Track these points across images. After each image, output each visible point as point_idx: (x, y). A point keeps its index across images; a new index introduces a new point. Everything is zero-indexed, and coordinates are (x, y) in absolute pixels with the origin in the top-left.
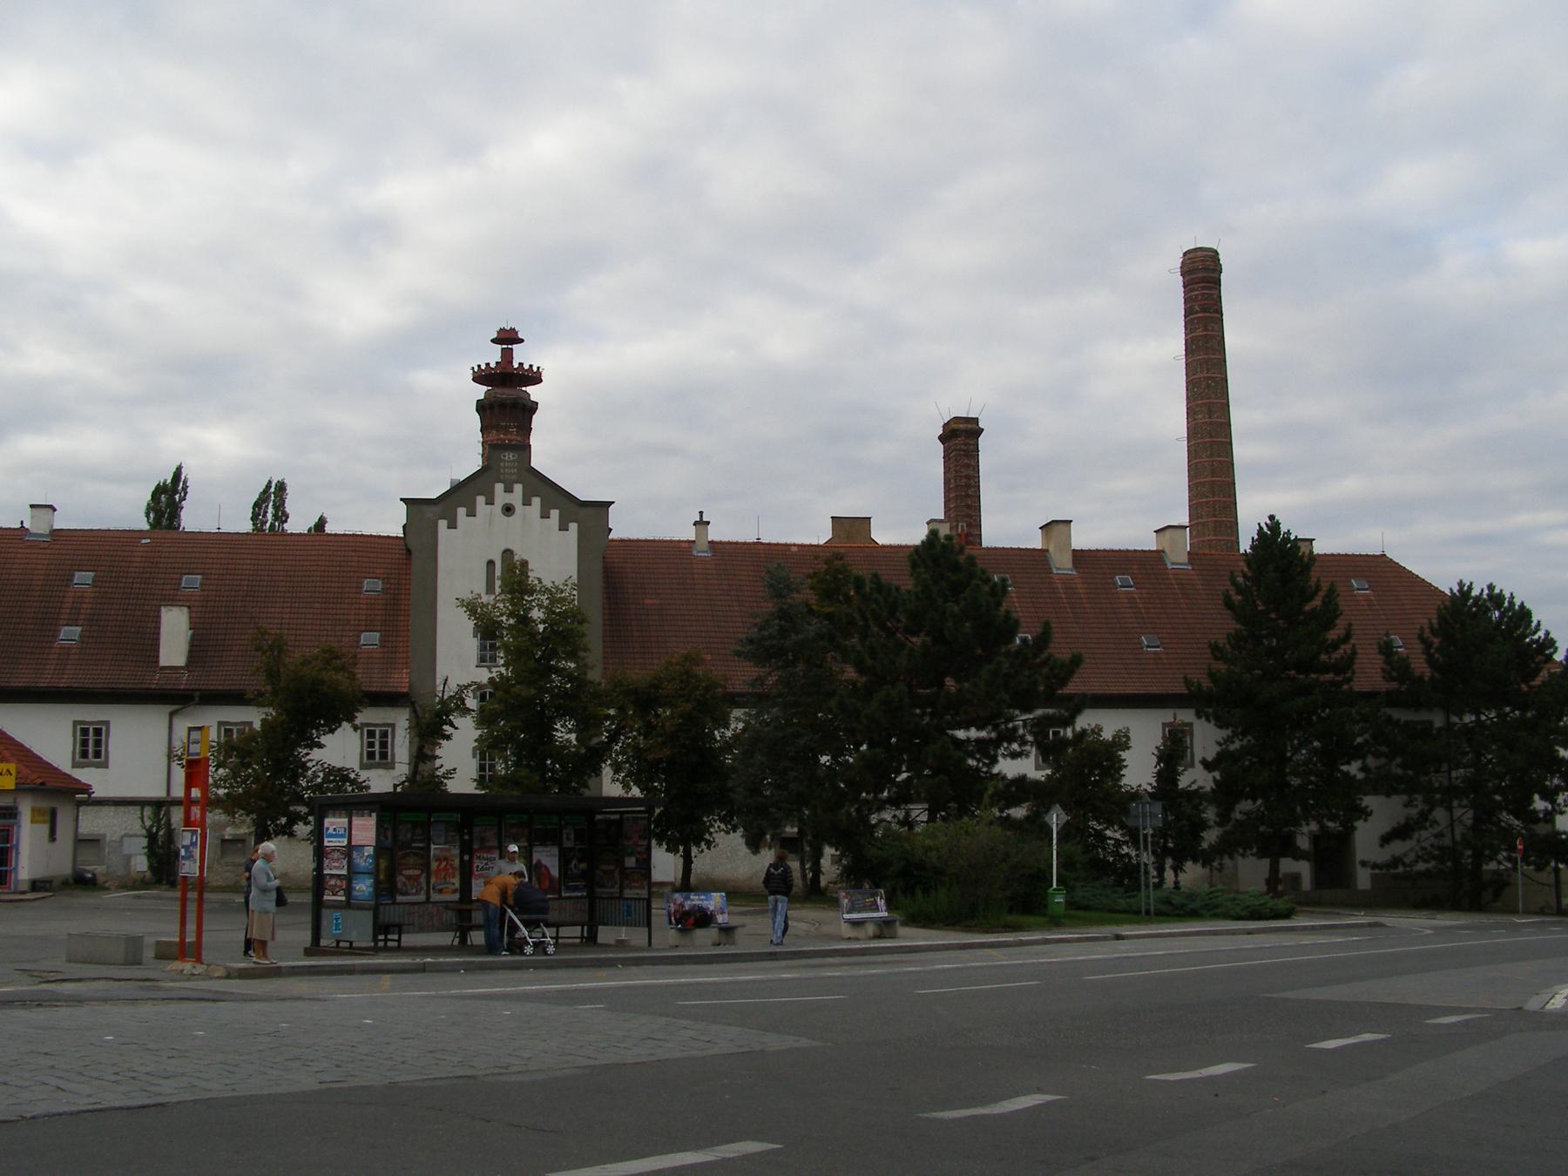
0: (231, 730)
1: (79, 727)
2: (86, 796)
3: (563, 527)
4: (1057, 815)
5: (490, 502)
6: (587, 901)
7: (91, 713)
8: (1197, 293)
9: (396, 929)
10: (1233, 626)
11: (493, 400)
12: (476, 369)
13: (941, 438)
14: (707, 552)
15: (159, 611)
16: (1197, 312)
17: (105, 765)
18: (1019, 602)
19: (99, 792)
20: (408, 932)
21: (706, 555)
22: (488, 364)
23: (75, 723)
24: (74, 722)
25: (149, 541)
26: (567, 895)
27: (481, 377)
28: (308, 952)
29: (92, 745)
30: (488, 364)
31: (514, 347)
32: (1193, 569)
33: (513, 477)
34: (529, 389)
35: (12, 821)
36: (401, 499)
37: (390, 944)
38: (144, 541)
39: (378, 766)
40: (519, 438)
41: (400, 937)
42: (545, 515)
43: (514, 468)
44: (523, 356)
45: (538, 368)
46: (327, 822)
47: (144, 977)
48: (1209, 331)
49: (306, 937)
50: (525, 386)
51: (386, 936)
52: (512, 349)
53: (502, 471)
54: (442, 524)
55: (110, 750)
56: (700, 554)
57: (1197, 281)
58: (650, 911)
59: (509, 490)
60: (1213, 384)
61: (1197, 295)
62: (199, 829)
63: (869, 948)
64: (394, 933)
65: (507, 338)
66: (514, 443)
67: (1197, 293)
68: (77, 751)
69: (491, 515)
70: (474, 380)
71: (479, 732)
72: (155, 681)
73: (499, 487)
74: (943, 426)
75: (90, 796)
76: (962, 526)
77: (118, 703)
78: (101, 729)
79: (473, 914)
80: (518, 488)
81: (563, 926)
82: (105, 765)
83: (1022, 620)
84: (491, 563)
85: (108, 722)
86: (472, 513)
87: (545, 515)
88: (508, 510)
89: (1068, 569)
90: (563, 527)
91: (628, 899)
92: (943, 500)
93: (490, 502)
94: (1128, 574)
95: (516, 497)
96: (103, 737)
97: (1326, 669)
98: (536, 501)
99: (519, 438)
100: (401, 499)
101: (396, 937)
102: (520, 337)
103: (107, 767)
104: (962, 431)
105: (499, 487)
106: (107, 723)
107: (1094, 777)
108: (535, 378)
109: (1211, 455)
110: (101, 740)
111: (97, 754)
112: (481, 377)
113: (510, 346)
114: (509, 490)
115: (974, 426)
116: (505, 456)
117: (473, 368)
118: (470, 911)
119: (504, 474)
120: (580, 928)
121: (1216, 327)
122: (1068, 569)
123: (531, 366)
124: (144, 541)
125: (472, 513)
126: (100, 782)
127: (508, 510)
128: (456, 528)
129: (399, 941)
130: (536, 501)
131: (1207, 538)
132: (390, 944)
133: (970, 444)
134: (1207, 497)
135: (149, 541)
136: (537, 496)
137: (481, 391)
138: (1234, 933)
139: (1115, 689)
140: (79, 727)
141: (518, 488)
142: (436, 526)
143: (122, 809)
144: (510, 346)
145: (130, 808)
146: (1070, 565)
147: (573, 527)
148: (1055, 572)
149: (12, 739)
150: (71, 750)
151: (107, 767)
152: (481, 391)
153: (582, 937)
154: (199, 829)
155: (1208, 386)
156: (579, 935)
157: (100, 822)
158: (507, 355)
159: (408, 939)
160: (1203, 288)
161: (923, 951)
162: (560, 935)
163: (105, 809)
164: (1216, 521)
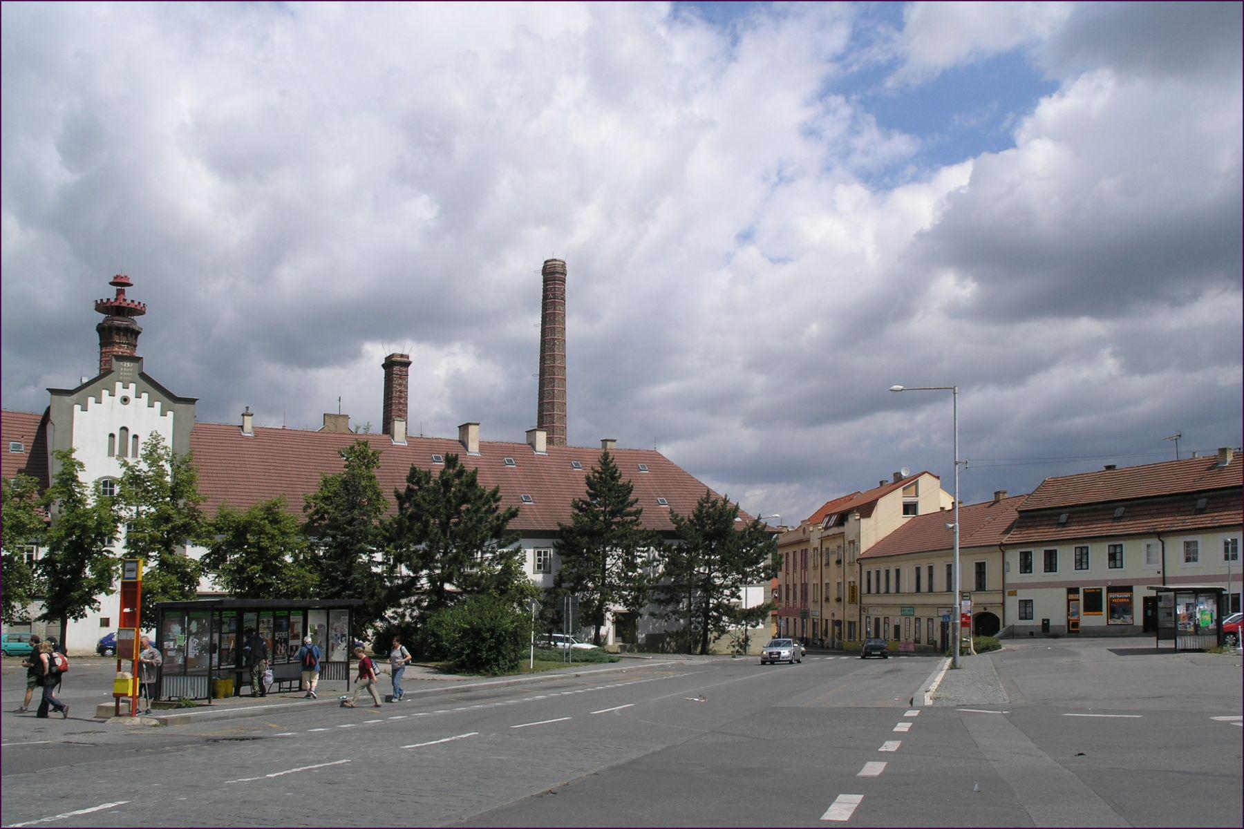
3: (163, 414)
5: (112, 394)
10: (488, 490)
12: (99, 302)
13: (383, 366)
14: (250, 433)
16: (551, 299)
21: (250, 435)
22: (102, 300)
27: (101, 307)
30: (108, 299)
31: (126, 288)
34: (136, 318)
36: (47, 389)
40: (129, 351)
42: (151, 405)
43: (130, 372)
46: (245, 617)
47: (231, 736)
52: (124, 290)
53: (121, 374)
54: (77, 408)
55: (533, 557)
58: (349, 671)
63: (479, 687)
65: (120, 284)
66: (124, 354)
69: (113, 403)
70: (96, 309)
71: (126, 551)
73: (119, 385)
74: (386, 358)
79: (243, 674)
80: (132, 386)
81: (294, 680)
83: (405, 481)
84: (112, 435)
86: (99, 401)
87: (151, 405)
88: (125, 400)
89: (476, 453)
90: (163, 414)
91: (334, 663)
92: (383, 404)
93: (112, 394)
97: (630, 514)
99: (129, 351)
100: (47, 389)
105: (119, 385)
107: (188, 578)
112: (101, 307)
115: (406, 359)
118: (241, 673)
119: (123, 376)
121: (561, 308)
122: (476, 453)
125: (99, 401)
127: (125, 400)
130: (145, 396)
136: (106, 389)
137: (101, 317)
141: (132, 386)
142: (72, 409)
146: (477, 451)
147: (170, 414)
152: (101, 317)
158: (120, 292)
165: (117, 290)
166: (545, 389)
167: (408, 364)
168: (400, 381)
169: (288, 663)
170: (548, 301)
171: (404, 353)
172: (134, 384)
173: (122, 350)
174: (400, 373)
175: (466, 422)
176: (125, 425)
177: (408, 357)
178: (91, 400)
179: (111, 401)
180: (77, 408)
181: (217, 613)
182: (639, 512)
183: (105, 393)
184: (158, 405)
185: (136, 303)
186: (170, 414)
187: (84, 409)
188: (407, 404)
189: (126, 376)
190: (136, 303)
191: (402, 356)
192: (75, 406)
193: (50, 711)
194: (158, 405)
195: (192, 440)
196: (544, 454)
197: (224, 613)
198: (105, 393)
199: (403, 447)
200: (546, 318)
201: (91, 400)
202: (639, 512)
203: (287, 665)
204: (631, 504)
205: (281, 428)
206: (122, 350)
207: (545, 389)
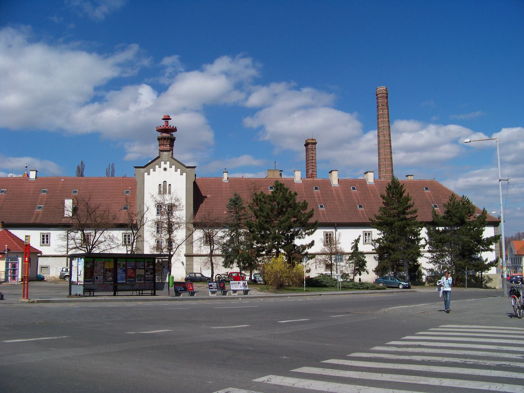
0: (331, 234)
1: (42, 235)
2: (40, 254)
3: (181, 174)
4: (306, 259)
5: (160, 167)
6: (153, 283)
7: (45, 232)
8: (380, 100)
9: (93, 291)
11: (162, 137)
15: (64, 200)
16: (380, 106)
17: (49, 245)
18: (319, 195)
19: (44, 253)
20: (97, 292)
23: (41, 233)
24: (363, 231)
25: (63, 180)
26: (137, 282)
28: (68, 297)
29: (45, 240)
32: (375, 185)
33: (167, 160)
34: (173, 133)
35: (17, 262)
36: (134, 167)
37: (91, 295)
38: (62, 180)
39: (45, 245)
41: (94, 293)
42: (176, 171)
43: (167, 157)
44: (172, 123)
45: (175, 127)
48: (384, 112)
49: (68, 294)
50: (172, 132)
51: (90, 293)
53: (163, 158)
54: (146, 174)
56: (225, 182)
57: (380, 97)
59: (165, 163)
60: (385, 128)
61: (380, 101)
62: (27, 263)
64: (92, 292)
66: (168, 149)
67: (380, 100)
68: (41, 241)
72: (64, 221)
73: (162, 163)
75: (41, 255)
76: (311, 172)
77: (26, 228)
78: (48, 235)
80: (168, 163)
82: (49, 245)
85: (372, 231)
86: (154, 170)
87: (176, 171)
89: (337, 185)
90: (181, 174)
93: (160, 167)
94: (355, 186)
95: (167, 165)
96: (49, 238)
98: (173, 167)
100: (134, 167)
101: (93, 293)
102: (170, 118)
103: (50, 246)
104: (311, 143)
105: (162, 163)
106: (371, 232)
108: (175, 130)
109: (385, 150)
110: (48, 238)
111: (47, 242)
113: (167, 121)
114: (165, 163)
116: (164, 153)
117: (156, 127)
119: (164, 159)
120: (151, 291)
123: (173, 126)
124: (62, 180)
125: (154, 170)
126: (45, 250)
128: (150, 175)
129: (93, 294)
131: (383, 175)
132: (91, 295)
133: (313, 147)
134: (383, 162)
135: (63, 180)
138: (359, 293)
139: (346, 221)
140: (42, 235)
141: (168, 163)
143: (54, 258)
144: (167, 121)
145: (56, 258)
147: (184, 174)
148: (332, 186)
149: (19, 238)
150: (40, 241)
151: (50, 246)
153: (152, 293)
154: (27, 263)
155: (384, 129)
156: (151, 293)
157: (48, 262)
159: (95, 294)
160: (382, 99)
161: (252, 298)
162: (143, 293)
163: (49, 258)
164: (386, 170)
165: (165, 122)
166: (380, 151)
167: (315, 143)
168: (312, 152)
169: (93, 284)
170: (379, 108)
171: (313, 138)
172: (169, 162)
173: (167, 147)
174: (312, 148)
175: (331, 171)
176: (164, 180)
177: (315, 140)
178: (151, 170)
179: (159, 170)
180: (146, 174)
181: (428, 241)
182: (415, 212)
183: (157, 166)
184: (179, 170)
185: (162, 126)
186: (184, 174)
187: (149, 174)
188: (316, 163)
189: (165, 159)
190: (159, 127)
191: (312, 140)
192: (145, 173)
193: (426, 275)
194: (179, 170)
195: (135, 191)
196: (373, 184)
197: (128, 260)
198: (157, 166)
199: (300, 184)
200: (379, 116)
201: (151, 170)
202: (415, 212)
203: (93, 285)
204: (409, 207)
205: (242, 177)
206: (167, 147)
207: (380, 151)
